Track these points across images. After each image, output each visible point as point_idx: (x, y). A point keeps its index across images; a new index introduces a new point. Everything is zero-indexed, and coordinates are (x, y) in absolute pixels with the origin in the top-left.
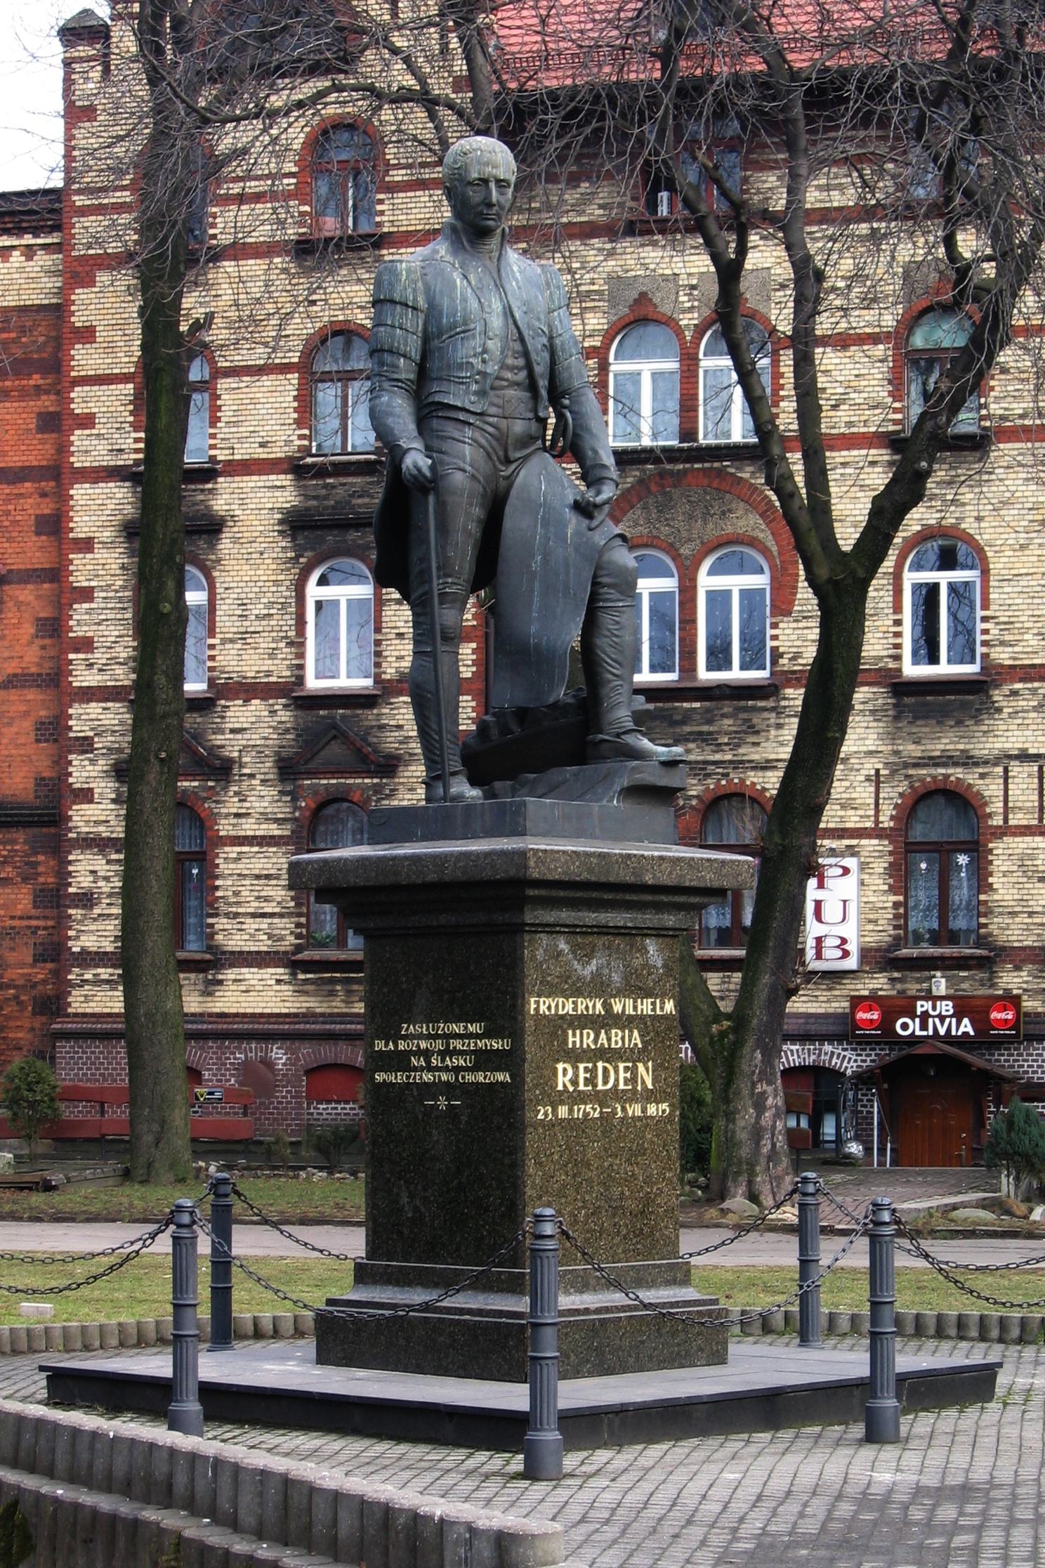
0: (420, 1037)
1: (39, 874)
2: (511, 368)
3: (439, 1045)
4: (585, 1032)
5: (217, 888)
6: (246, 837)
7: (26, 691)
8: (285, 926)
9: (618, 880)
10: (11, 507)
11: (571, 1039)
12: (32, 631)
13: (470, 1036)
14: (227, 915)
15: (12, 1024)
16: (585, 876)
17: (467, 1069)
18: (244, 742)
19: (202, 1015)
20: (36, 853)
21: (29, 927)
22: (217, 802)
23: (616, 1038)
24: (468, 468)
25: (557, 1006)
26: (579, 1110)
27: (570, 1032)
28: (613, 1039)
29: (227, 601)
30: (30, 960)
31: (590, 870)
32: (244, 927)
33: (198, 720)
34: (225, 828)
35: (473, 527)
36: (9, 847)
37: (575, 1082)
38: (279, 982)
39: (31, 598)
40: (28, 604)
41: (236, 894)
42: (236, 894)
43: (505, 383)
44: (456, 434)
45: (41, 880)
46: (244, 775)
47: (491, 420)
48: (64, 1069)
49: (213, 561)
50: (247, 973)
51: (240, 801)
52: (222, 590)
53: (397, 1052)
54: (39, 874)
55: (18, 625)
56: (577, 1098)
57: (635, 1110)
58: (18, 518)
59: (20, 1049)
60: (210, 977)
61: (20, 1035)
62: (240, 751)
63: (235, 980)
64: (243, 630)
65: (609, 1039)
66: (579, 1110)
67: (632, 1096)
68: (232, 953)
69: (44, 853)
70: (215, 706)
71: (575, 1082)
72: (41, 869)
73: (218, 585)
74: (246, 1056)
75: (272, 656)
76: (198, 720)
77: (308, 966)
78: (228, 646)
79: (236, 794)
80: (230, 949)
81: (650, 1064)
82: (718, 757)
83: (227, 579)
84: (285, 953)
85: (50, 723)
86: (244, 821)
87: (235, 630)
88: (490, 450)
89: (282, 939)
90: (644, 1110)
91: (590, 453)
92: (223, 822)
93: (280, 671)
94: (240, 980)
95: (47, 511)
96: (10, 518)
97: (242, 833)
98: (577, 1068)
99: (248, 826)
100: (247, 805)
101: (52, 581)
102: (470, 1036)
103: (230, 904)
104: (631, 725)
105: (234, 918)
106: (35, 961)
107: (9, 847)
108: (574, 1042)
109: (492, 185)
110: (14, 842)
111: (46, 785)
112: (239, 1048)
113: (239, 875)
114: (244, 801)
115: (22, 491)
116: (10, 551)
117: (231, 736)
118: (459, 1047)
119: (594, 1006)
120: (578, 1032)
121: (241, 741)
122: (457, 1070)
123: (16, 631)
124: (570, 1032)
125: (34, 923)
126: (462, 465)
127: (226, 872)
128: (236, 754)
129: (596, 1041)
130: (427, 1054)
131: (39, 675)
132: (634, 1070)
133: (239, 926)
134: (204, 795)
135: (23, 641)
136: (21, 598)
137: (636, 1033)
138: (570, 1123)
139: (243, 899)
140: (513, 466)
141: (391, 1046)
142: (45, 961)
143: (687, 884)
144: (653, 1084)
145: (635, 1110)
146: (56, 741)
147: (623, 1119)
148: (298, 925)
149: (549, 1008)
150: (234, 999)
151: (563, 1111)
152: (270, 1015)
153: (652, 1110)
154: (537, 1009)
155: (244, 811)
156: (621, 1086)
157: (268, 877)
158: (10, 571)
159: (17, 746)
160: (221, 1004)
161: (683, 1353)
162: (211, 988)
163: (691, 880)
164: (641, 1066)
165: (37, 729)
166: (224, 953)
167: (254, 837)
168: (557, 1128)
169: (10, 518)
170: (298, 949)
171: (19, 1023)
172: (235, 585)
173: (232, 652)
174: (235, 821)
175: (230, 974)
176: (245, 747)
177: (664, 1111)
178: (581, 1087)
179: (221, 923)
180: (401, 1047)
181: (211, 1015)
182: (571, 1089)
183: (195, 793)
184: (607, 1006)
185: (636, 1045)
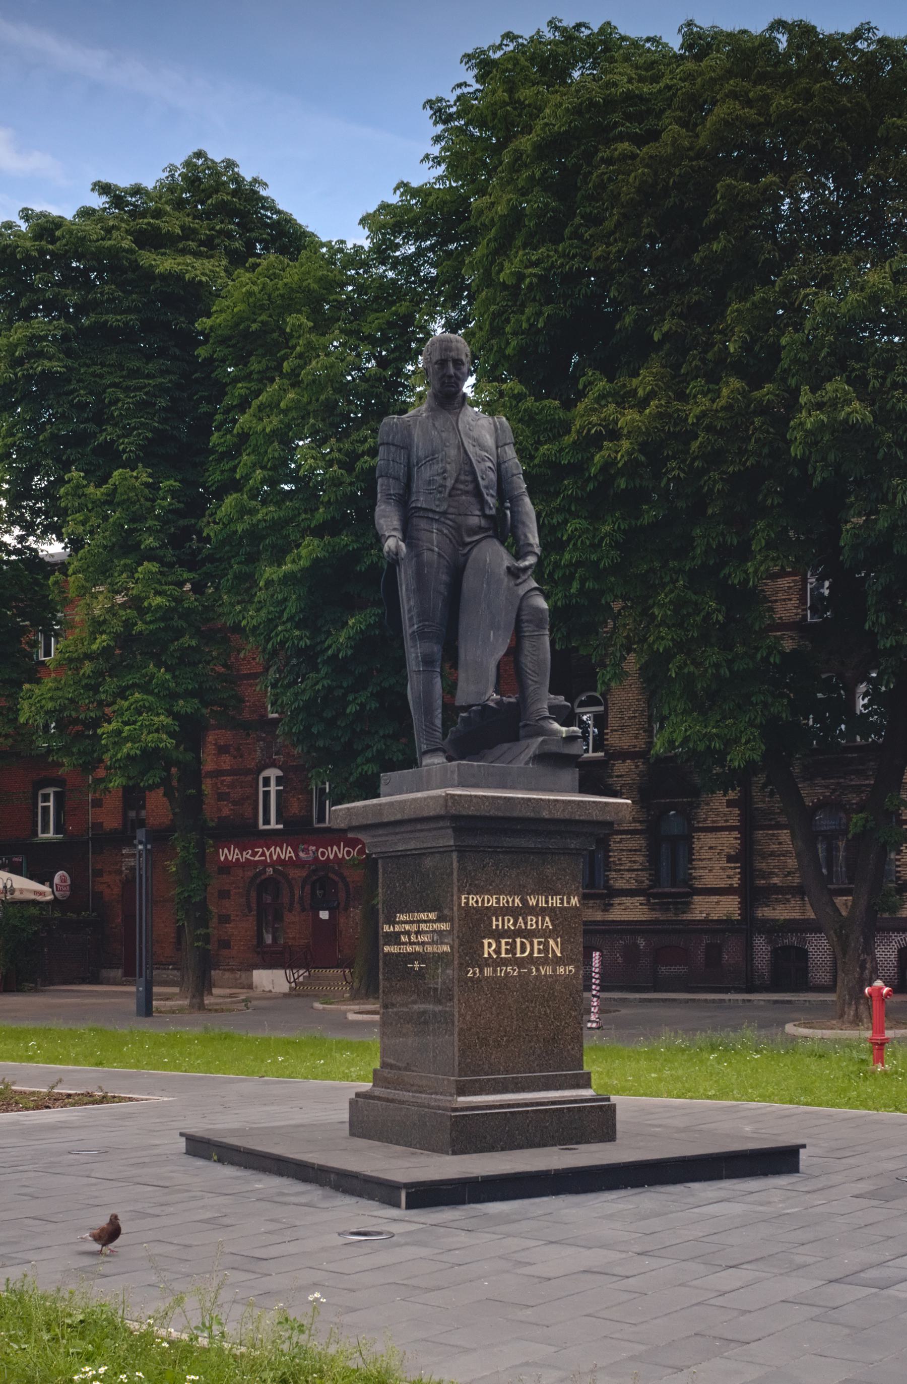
0: (406, 922)
2: (463, 482)
3: (414, 927)
4: (506, 918)
5: (610, 857)
8: (644, 876)
11: (494, 923)
14: (615, 871)
17: (428, 943)
19: (603, 921)
23: (532, 922)
24: (436, 549)
25: (483, 901)
26: (501, 971)
27: (494, 919)
28: (529, 923)
35: (442, 588)
37: (497, 951)
38: (641, 904)
41: (620, 859)
42: (620, 859)
43: (459, 492)
47: (450, 516)
50: (624, 899)
53: (394, 932)
57: (545, 970)
63: (619, 904)
65: (526, 924)
66: (501, 971)
67: (545, 961)
68: (618, 890)
71: (497, 951)
75: (636, 738)
77: (655, 896)
81: (559, 940)
82: (867, 782)
84: (644, 889)
88: (450, 536)
89: (643, 882)
90: (554, 970)
91: (522, 537)
93: (641, 744)
98: (500, 942)
103: (617, 865)
104: (547, 714)
108: (497, 926)
109: (451, 365)
118: (425, 929)
119: (513, 901)
120: (500, 919)
121: (621, 781)
124: (494, 919)
126: (430, 546)
129: (515, 924)
130: (408, 933)
132: (546, 945)
137: (547, 919)
138: (494, 979)
140: (469, 547)
141: (392, 929)
143: (577, 818)
144: (561, 953)
145: (545, 970)
147: (536, 977)
148: (650, 875)
149: (477, 902)
151: (488, 971)
152: (637, 921)
153: (561, 970)
154: (467, 903)
156: (536, 955)
157: (635, 850)
163: (580, 816)
164: (551, 942)
167: (628, 830)
170: (650, 887)
175: (617, 901)
177: (570, 971)
178: (503, 955)
180: (396, 930)
182: (495, 956)
184: (524, 901)
185: (548, 927)
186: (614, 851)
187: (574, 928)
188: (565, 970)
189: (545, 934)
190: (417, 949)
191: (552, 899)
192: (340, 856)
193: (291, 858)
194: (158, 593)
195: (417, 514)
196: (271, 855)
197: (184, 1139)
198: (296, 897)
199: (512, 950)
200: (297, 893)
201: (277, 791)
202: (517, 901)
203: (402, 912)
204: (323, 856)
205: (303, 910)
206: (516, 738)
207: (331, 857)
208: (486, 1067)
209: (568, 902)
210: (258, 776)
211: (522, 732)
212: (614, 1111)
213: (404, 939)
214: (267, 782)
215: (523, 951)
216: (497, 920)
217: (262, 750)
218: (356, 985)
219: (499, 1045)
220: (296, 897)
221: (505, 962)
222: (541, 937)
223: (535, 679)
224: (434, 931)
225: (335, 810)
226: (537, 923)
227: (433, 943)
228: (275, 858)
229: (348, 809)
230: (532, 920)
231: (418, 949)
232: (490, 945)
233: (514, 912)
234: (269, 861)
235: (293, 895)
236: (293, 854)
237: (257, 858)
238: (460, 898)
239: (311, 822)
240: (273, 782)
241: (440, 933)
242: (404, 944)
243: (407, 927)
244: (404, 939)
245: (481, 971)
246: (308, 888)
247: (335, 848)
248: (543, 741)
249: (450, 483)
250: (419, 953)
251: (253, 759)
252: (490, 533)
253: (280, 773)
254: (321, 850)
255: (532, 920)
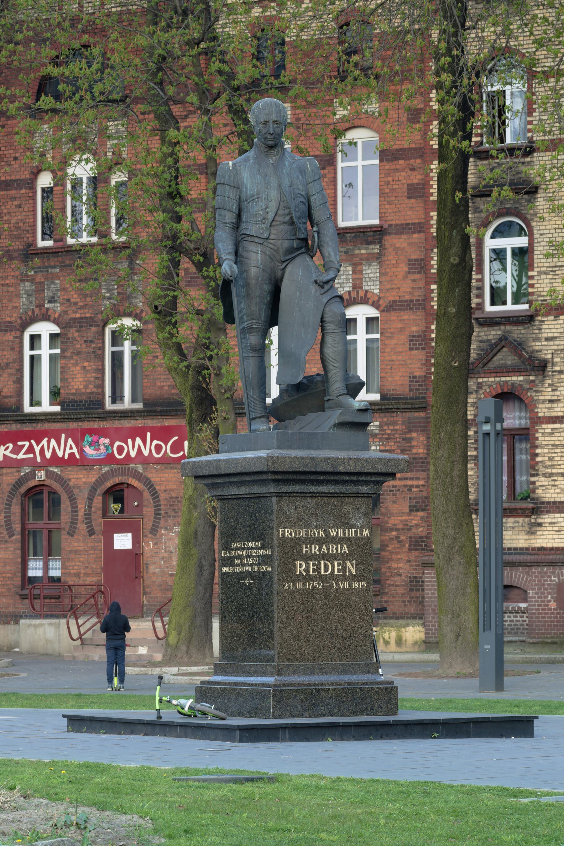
0: (239, 549)
1: (413, 447)
3: (245, 553)
6: (557, 417)
7: (402, 313)
9: (323, 470)
10: (390, 179)
11: (304, 549)
12: (406, 269)
13: (256, 548)
14: (544, 475)
15: (394, 557)
16: (302, 469)
17: (255, 565)
18: (555, 347)
19: (527, 549)
20: (410, 431)
21: (405, 486)
22: (536, 391)
23: (333, 549)
25: (296, 533)
26: (309, 585)
29: (542, 244)
30: (407, 510)
31: (306, 466)
32: (557, 483)
33: (523, 331)
34: (542, 411)
36: (391, 428)
37: (307, 570)
39: (405, 245)
40: (403, 249)
41: (551, 459)
42: (551, 459)
44: (254, 249)
45: (415, 451)
46: (556, 371)
48: (431, 590)
49: (531, 214)
51: (553, 390)
52: (538, 236)
54: (413, 447)
55: (396, 265)
56: (307, 578)
58: (395, 187)
59: (400, 575)
60: (533, 521)
61: (400, 565)
62: (553, 354)
63: (550, 523)
64: (553, 264)
65: (328, 550)
66: (309, 585)
67: (344, 578)
68: (549, 503)
69: (417, 431)
70: (534, 321)
71: (307, 570)
72: (414, 443)
73: (535, 232)
74: (559, 579)
76: (523, 331)
78: (543, 277)
79: (550, 385)
80: (546, 500)
83: (542, 227)
85: (419, 336)
86: (555, 405)
87: (548, 265)
90: (350, 585)
92: (541, 406)
94: (554, 523)
95: (415, 181)
96: (390, 187)
97: (554, 414)
98: (308, 563)
99: (558, 409)
100: (558, 393)
101: (419, 232)
102: (256, 548)
103: (546, 467)
105: (550, 477)
106: (411, 510)
107: (391, 428)
108: (306, 551)
110: (394, 423)
111: (417, 382)
112: (553, 573)
113: (553, 445)
114: (556, 390)
115: (398, 167)
116: (389, 211)
117: (546, 343)
119: (319, 533)
122: (252, 565)
123: (395, 269)
125: (409, 483)
127: (544, 443)
128: (549, 356)
129: (320, 550)
130: (240, 557)
131: (412, 301)
133: (553, 483)
134: (528, 386)
135: (400, 276)
136: (398, 245)
137: (345, 546)
138: (304, 591)
139: (556, 463)
142: (417, 510)
146: (423, 349)
147: (336, 590)
149: (291, 534)
150: (550, 537)
151: (299, 585)
153: (355, 585)
154: (283, 535)
155: (555, 398)
158: (390, 226)
159: (396, 353)
160: (541, 541)
161: (369, 708)
162: (534, 529)
164: (348, 564)
165: (410, 341)
166: (543, 503)
168: (296, 594)
169: (390, 187)
171: (399, 556)
172: (547, 231)
173: (546, 281)
174: (549, 405)
175: (546, 518)
176: (555, 350)
177: (363, 586)
179: (540, 481)
180: (231, 555)
181: (534, 549)
183: (521, 386)
184: (327, 534)
185: (345, 552)
186: (542, 447)
187: (366, 553)
188: (359, 585)
189: (343, 558)
190: (247, 569)
191: (349, 531)
192: (146, 453)
193: (72, 455)
194: (31, 275)
195: (246, 239)
196: (42, 451)
197: (66, 719)
198: (81, 514)
199: (317, 569)
200: (82, 507)
201: (51, 355)
202: (321, 533)
203: (235, 541)
204: (120, 453)
205: (91, 532)
206: (322, 409)
207: (133, 454)
208: (298, 656)
209: (361, 534)
210: (23, 332)
211: (326, 405)
212: (397, 692)
213: (237, 561)
214: (35, 339)
215: (326, 570)
216: (306, 547)
217: (29, 295)
218: (173, 639)
219: (308, 640)
220: (81, 514)
221: (311, 579)
222: (340, 560)
223: (336, 365)
224: (258, 556)
225: (184, 463)
226: (337, 549)
227: (259, 564)
228: (48, 455)
229: (194, 462)
230: (333, 547)
231: (248, 569)
232: (301, 566)
233: (320, 542)
234: (39, 459)
235: (75, 510)
236: (75, 450)
237: (21, 456)
238: (278, 531)
239: (101, 403)
240: (45, 341)
241: (264, 556)
242: (237, 565)
243: (240, 553)
244: (237, 561)
245: (294, 585)
246: (98, 500)
247: (138, 441)
248: (341, 413)
249: (271, 216)
250: (249, 572)
251: (16, 307)
252: (303, 250)
253: (55, 329)
254: (117, 443)
255: (333, 547)
